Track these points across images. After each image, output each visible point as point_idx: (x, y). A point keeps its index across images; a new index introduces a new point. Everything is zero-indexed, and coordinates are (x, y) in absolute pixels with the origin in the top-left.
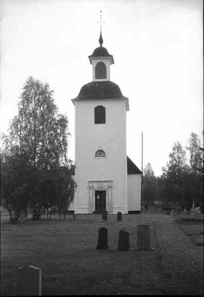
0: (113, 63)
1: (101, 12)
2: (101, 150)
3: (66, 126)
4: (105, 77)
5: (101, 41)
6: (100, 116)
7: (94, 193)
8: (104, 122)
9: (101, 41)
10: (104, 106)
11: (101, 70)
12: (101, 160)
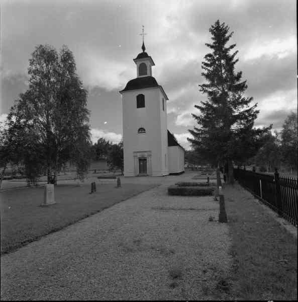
0: (154, 65)
3: (83, 90)
4: (146, 74)
5: (143, 48)
6: (141, 102)
7: (138, 160)
8: (144, 107)
9: (143, 48)
11: (142, 69)
12: (142, 135)
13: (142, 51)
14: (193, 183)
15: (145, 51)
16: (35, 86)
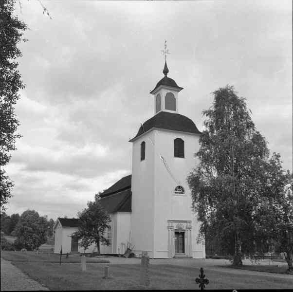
1: (166, 42)
2: (180, 187)
5: (166, 71)
8: (176, 156)
9: (166, 71)
10: (183, 139)
13: (163, 76)
14: (245, 269)
15: (169, 76)
16: (17, 87)
